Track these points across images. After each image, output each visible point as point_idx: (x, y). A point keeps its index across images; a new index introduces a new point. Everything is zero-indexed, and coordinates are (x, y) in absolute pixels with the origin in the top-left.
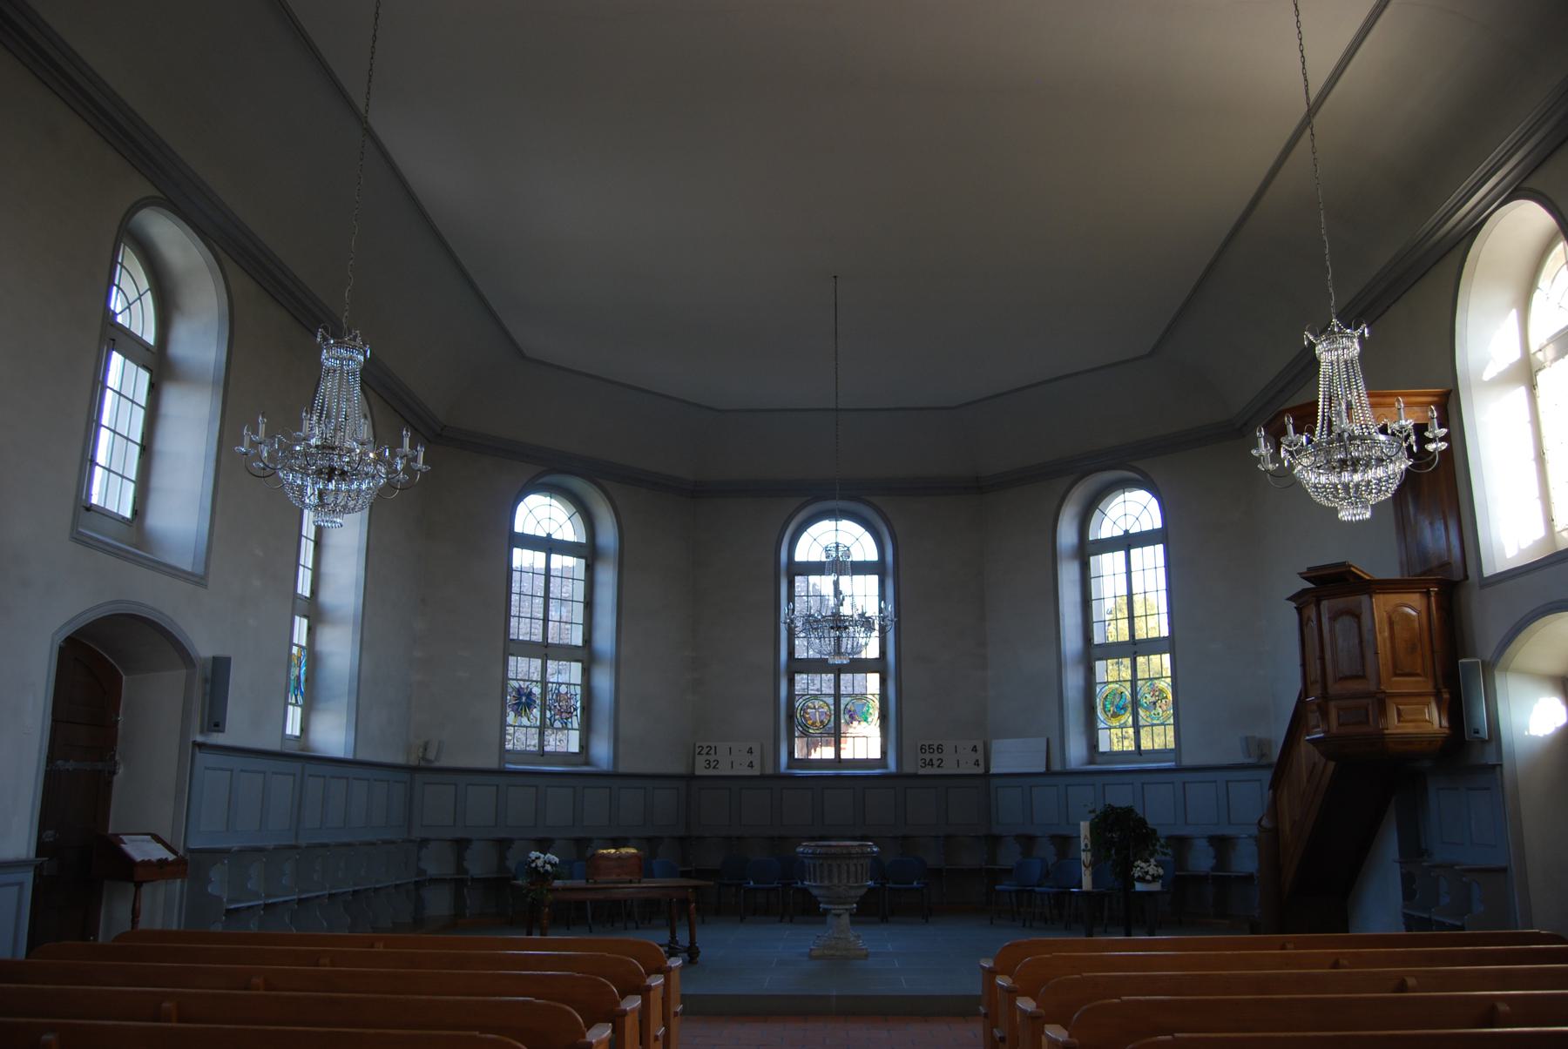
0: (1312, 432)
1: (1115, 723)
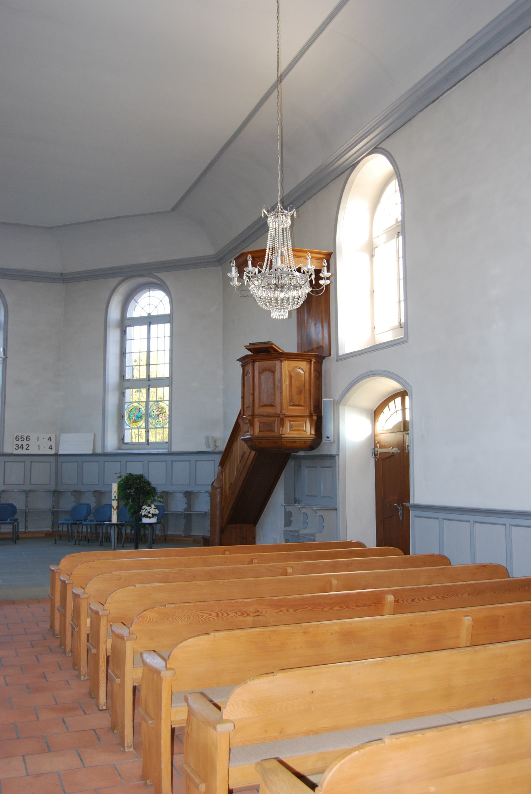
0: (261, 267)
1: (134, 426)
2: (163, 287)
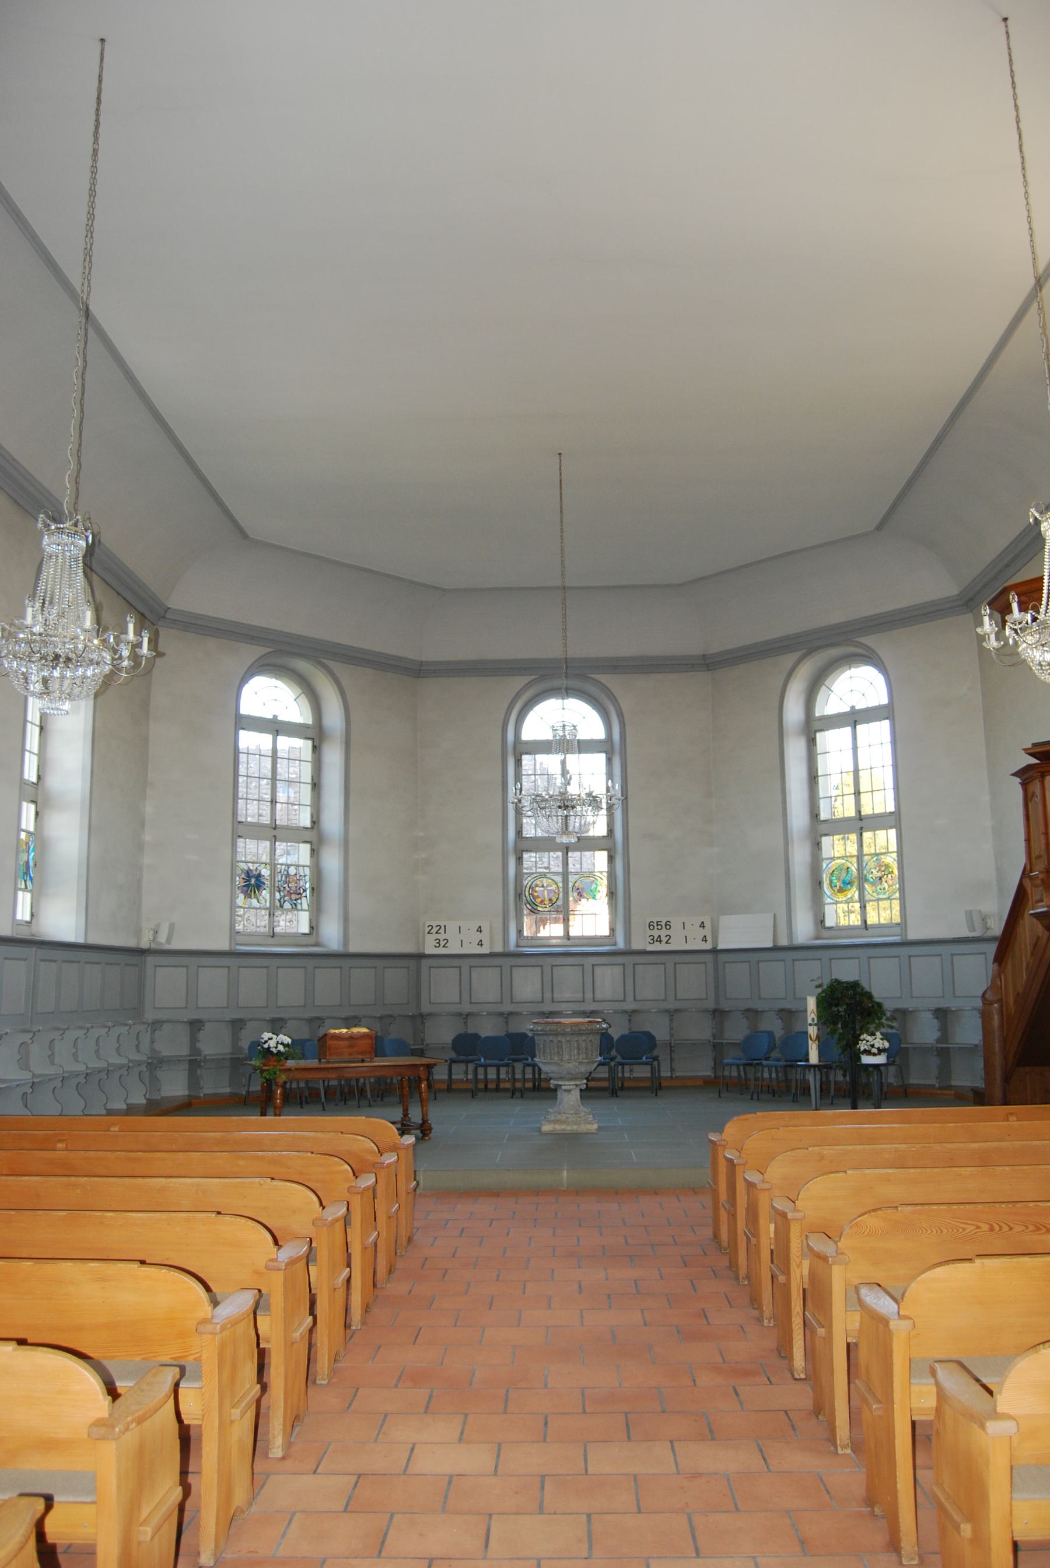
1: (841, 898)
2: (870, 658)
